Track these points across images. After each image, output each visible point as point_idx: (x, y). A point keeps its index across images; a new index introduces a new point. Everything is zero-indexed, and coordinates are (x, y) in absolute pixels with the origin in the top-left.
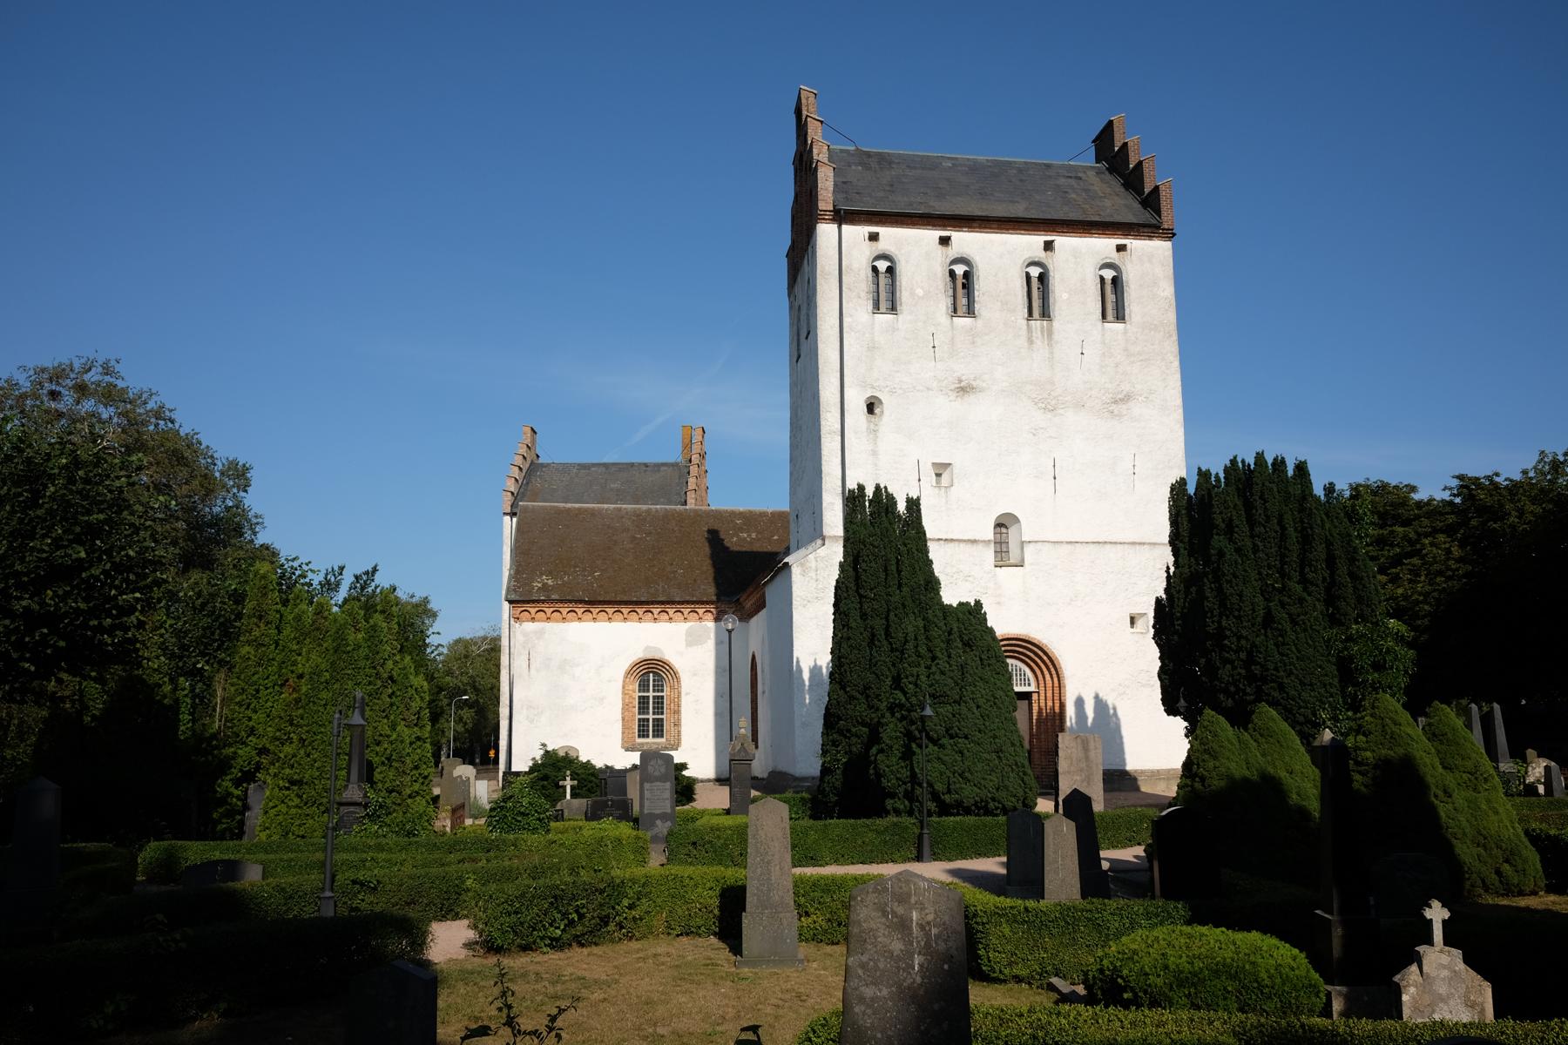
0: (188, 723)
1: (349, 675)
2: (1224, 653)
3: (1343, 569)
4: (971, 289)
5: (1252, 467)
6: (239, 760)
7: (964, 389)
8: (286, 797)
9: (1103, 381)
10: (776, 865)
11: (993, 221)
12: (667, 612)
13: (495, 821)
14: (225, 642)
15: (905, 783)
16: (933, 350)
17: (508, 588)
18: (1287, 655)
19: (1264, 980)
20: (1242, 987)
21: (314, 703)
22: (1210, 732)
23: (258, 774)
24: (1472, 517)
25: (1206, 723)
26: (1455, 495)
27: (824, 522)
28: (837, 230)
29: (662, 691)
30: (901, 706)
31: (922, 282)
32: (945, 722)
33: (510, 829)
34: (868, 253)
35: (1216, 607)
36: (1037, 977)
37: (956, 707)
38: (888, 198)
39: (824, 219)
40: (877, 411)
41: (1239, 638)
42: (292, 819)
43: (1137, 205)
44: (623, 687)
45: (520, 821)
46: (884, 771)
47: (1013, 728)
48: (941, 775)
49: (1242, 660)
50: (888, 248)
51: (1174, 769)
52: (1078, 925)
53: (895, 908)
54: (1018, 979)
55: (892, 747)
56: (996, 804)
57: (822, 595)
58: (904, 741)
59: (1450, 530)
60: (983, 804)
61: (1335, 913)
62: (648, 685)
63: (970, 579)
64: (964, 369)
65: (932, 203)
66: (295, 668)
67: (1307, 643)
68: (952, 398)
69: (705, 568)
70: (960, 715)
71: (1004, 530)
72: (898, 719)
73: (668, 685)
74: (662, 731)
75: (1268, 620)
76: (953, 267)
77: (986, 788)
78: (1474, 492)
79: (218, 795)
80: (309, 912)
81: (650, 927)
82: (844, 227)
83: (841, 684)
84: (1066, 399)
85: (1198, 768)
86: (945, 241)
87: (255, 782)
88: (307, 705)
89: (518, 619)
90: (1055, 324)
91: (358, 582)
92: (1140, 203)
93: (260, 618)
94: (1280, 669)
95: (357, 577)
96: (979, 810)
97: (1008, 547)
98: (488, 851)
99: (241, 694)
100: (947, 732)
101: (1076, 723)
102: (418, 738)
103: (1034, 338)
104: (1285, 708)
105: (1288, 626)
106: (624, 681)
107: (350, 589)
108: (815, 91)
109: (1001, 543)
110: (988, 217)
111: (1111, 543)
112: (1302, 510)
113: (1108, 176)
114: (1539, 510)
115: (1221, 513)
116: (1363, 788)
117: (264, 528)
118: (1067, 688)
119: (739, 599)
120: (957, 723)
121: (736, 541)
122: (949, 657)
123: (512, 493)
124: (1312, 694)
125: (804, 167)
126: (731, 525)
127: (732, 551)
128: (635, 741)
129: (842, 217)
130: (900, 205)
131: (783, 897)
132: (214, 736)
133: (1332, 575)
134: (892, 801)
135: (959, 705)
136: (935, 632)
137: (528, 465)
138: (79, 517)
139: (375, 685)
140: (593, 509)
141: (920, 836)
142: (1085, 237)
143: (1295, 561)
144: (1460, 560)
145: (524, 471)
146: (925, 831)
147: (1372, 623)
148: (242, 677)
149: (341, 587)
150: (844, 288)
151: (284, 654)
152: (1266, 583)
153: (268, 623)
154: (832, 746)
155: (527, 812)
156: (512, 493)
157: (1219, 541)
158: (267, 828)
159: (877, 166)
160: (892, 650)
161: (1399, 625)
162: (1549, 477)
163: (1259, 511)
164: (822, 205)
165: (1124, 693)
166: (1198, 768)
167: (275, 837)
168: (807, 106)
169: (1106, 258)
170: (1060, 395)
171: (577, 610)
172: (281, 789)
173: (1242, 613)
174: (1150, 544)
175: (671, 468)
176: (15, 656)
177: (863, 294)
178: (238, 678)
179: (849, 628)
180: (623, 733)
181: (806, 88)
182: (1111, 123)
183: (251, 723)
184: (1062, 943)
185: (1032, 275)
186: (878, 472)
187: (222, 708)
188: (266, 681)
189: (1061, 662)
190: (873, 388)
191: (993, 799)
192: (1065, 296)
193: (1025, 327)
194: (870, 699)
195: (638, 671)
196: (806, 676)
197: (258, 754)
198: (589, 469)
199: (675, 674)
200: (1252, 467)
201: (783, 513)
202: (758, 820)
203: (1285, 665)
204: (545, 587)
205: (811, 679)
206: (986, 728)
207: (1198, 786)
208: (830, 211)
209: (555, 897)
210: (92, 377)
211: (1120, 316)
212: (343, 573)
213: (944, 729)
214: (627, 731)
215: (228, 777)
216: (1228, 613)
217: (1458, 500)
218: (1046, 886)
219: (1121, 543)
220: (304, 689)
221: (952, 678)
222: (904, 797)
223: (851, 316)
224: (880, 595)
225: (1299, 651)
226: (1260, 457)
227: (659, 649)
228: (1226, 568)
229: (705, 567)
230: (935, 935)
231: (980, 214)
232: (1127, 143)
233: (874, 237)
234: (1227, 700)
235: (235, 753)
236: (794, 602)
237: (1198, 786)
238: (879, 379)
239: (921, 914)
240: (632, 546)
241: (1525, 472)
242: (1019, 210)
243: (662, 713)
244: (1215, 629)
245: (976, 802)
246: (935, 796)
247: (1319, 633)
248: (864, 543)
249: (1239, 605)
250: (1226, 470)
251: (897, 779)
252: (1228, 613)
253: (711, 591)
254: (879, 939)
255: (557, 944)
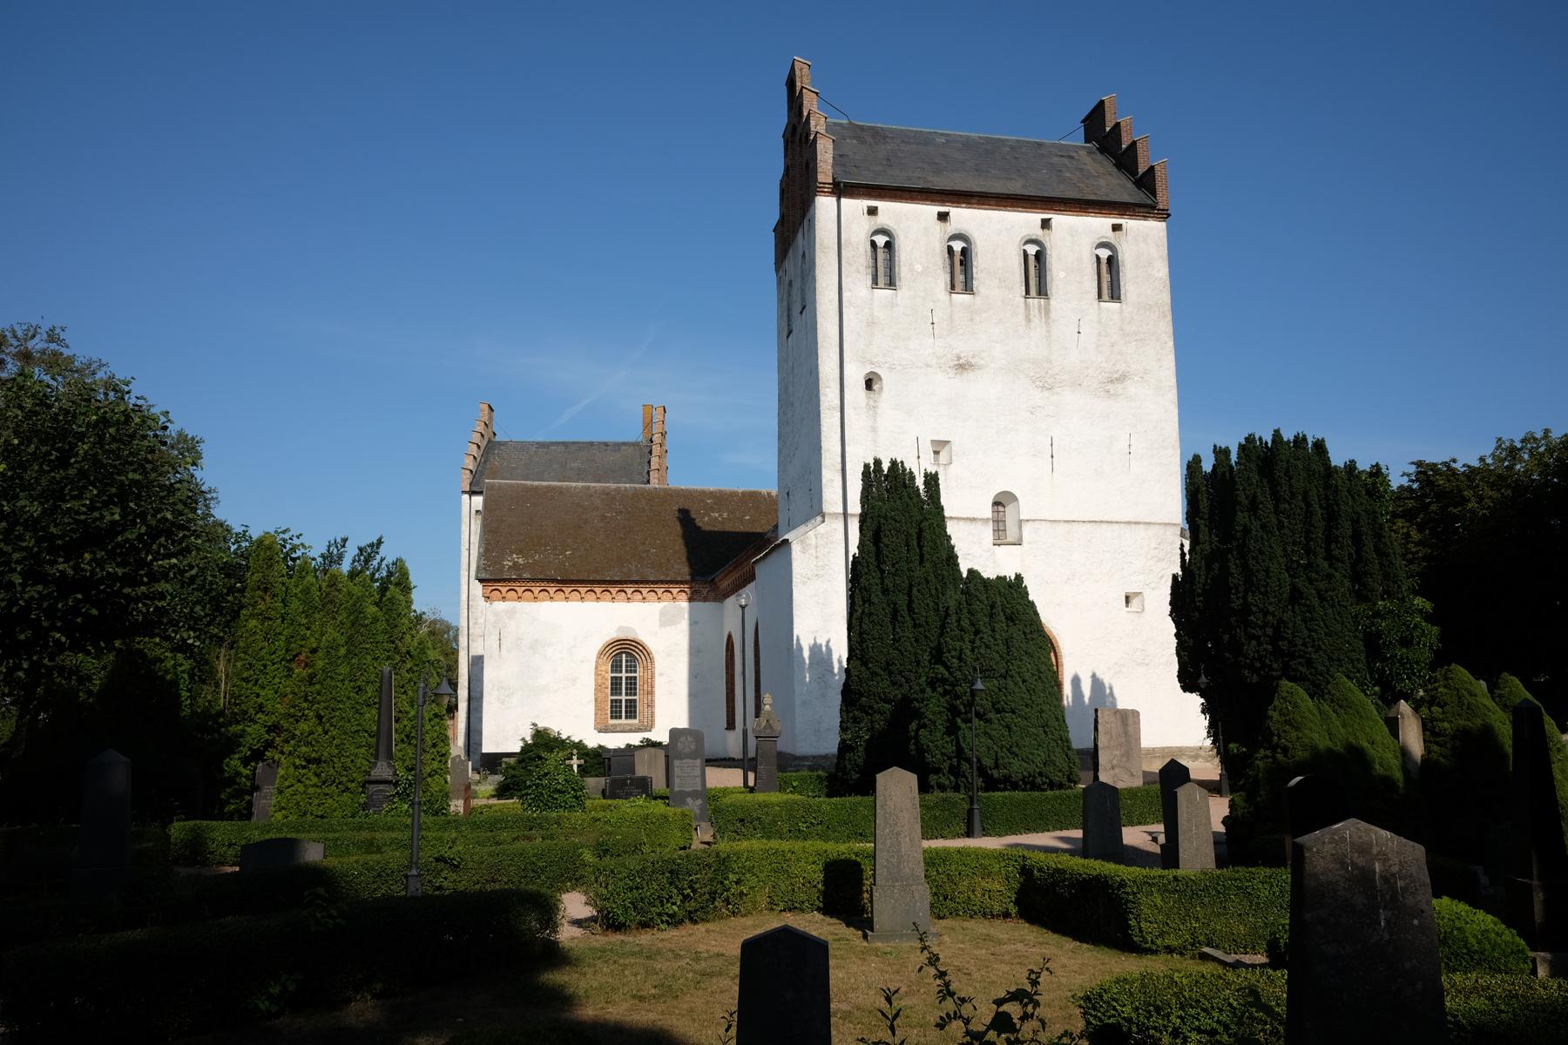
0: (186, 700)
1: (367, 649)
2: (1249, 629)
3: (1369, 544)
4: (969, 265)
5: (1269, 445)
6: (249, 738)
7: (962, 367)
8: (303, 776)
9: (1100, 360)
10: (906, 836)
11: (992, 197)
12: (641, 592)
13: (531, 799)
14: (217, 616)
15: (950, 758)
16: (931, 326)
17: (478, 567)
18: (1316, 631)
19: (1473, 946)
20: (1452, 954)
21: (332, 678)
22: (1290, 703)
23: (267, 753)
24: (1430, 503)
25: (1284, 694)
26: (1412, 481)
27: (824, 499)
28: (836, 203)
29: (635, 672)
30: (944, 681)
31: (920, 257)
32: (991, 696)
33: (547, 807)
34: (867, 227)
35: (1241, 583)
36: (1190, 947)
37: (1002, 681)
38: (885, 172)
39: (823, 192)
40: (875, 387)
41: (1266, 613)
42: (310, 798)
43: (1130, 185)
44: (596, 668)
45: (556, 799)
46: (928, 746)
47: (1056, 703)
48: (989, 750)
49: (1268, 636)
50: (888, 222)
51: (1168, 748)
52: (1229, 894)
53: (1355, 859)
54: (1170, 950)
55: (935, 722)
56: (1044, 779)
57: (822, 572)
58: (947, 716)
59: (1408, 515)
60: (1030, 779)
61: (1535, 877)
62: (621, 666)
63: (969, 557)
64: (963, 346)
65: (930, 178)
66: (304, 642)
67: (1335, 619)
68: (951, 375)
69: (677, 547)
70: (1006, 689)
71: (1001, 508)
72: (940, 694)
73: (641, 665)
74: (635, 712)
75: (1296, 596)
76: (951, 243)
77: (1033, 762)
78: (1431, 478)
79: (226, 775)
80: (398, 890)
81: (754, 903)
82: (844, 201)
83: (862, 661)
84: (1063, 378)
85: (1279, 739)
86: (943, 217)
87: (263, 761)
88: (324, 680)
89: (488, 598)
90: (1053, 302)
91: (362, 554)
92: (1134, 183)
93: (266, 590)
94: (1308, 645)
95: (361, 550)
96: (1026, 785)
97: (1005, 526)
98: (531, 829)
99: (248, 669)
100: (993, 707)
101: (1073, 701)
102: (436, 715)
103: (1031, 317)
104: (1314, 684)
105: (1316, 601)
106: (597, 662)
107: (354, 561)
108: (808, 63)
109: (998, 521)
110: (986, 193)
111: (1108, 522)
112: (1327, 487)
113: (1099, 157)
114: (1495, 495)
115: (1244, 490)
116: (1442, 760)
117: (218, 503)
118: (1065, 667)
119: (713, 580)
120: (1004, 698)
121: (708, 521)
122: (993, 631)
123: (471, 471)
124: (1340, 669)
125: (798, 140)
126: (702, 505)
127: (705, 531)
128: (607, 722)
129: (841, 190)
130: (898, 179)
131: (913, 870)
132: (221, 713)
133: (1358, 552)
134: (935, 777)
135: (1005, 679)
136: (977, 606)
137: (485, 443)
138: (115, 476)
139: (394, 660)
140: (561, 487)
141: (970, 812)
142: (1081, 216)
143: (1321, 538)
144: (1417, 544)
145: (482, 449)
146: (976, 806)
147: (1398, 599)
148: (250, 652)
149: (344, 559)
150: (843, 263)
151: (292, 628)
152: (1292, 559)
153: (274, 595)
154: (853, 722)
155: (564, 789)
156: (471, 471)
157: (1242, 517)
158: (283, 808)
159: (871, 140)
160: (915, 626)
161: (1424, 602)
162: (1506, 464)
163: (1284, 488)
164: (821, 178)
165: (1120, 672)
166: (1279, 739)
167: (293, 818)
168: (801, 77)
169: (1102, 237)
170: (1057, 374)
171: (548, 589)
172: (296, 767)
173: (1269, 589)
174: (1145, 523)
175: (632, 447)
176: (45, 624)
177: (862, 269)
178: (245, 653)
179: (871, 603)
180: (596, 714)
181: (800, 59)
182: (1102, 102)
183: (259, 700)
184: (1214, 912)
185: (1029, 252)
186: (878, 449)
187: (226, 683)
188: (273, 656)
189: (1058, 640)
190: (872, 363)
191: (1040, 774)
192: (1062, 274)
193: (1023, 305)
194: (893, 675)
195: (611, 651)
196: (806, 654)
197: (267, 732)
198: (548, 448)
199: (648, 655)
200: (1269, 445)
201: (753, 497)
202: (886, 790)
203: (1313, 641)
204: (516, 566)
205: (811, 657)
206: (1033, 702)
207: (1280, 756)
208: (829, 184)
209: (671, 872)
210: (36, 345)
211: (1115, 296)
212: (346, 545)
213: (991, 704)
214: (599, 712)
215: (237, 756)
216: (1254, 589)
217: (1415, 486)
218: (1181, 855)
219: (1117, 523)
220: (320, 664)
221: (997, 652)
222: (949, 772)
223: (850, 290)
224: (902, 571)
225: (1327, 628)
226: (1277, 435)
227: (633, 630)
228: (1252, 545)
229: (678, 548)
230: (1401, 887)
231: (978, 190)
232: (1120, 123)
233: (872, 211)
234: (1252, 676)
235: (244, 731)
236: (794, 579)
237: (1280, 756)
238: (878, 355)
239: (1384, 866)
240: (602, 525)
241: (1482, 459)
242: (1016, 187)
243: (635, 694)
244: (1240, 605)
245: (1024, 777)
246: (982, 771)
247: (1347, 609)
248: (885, 518)
249: (1265, 581)
250: (1242, 448)
251: (942, 754)
252: (1254, 589)
253: (684, 571)
254: (1339, 893)
255: (674, 921)
